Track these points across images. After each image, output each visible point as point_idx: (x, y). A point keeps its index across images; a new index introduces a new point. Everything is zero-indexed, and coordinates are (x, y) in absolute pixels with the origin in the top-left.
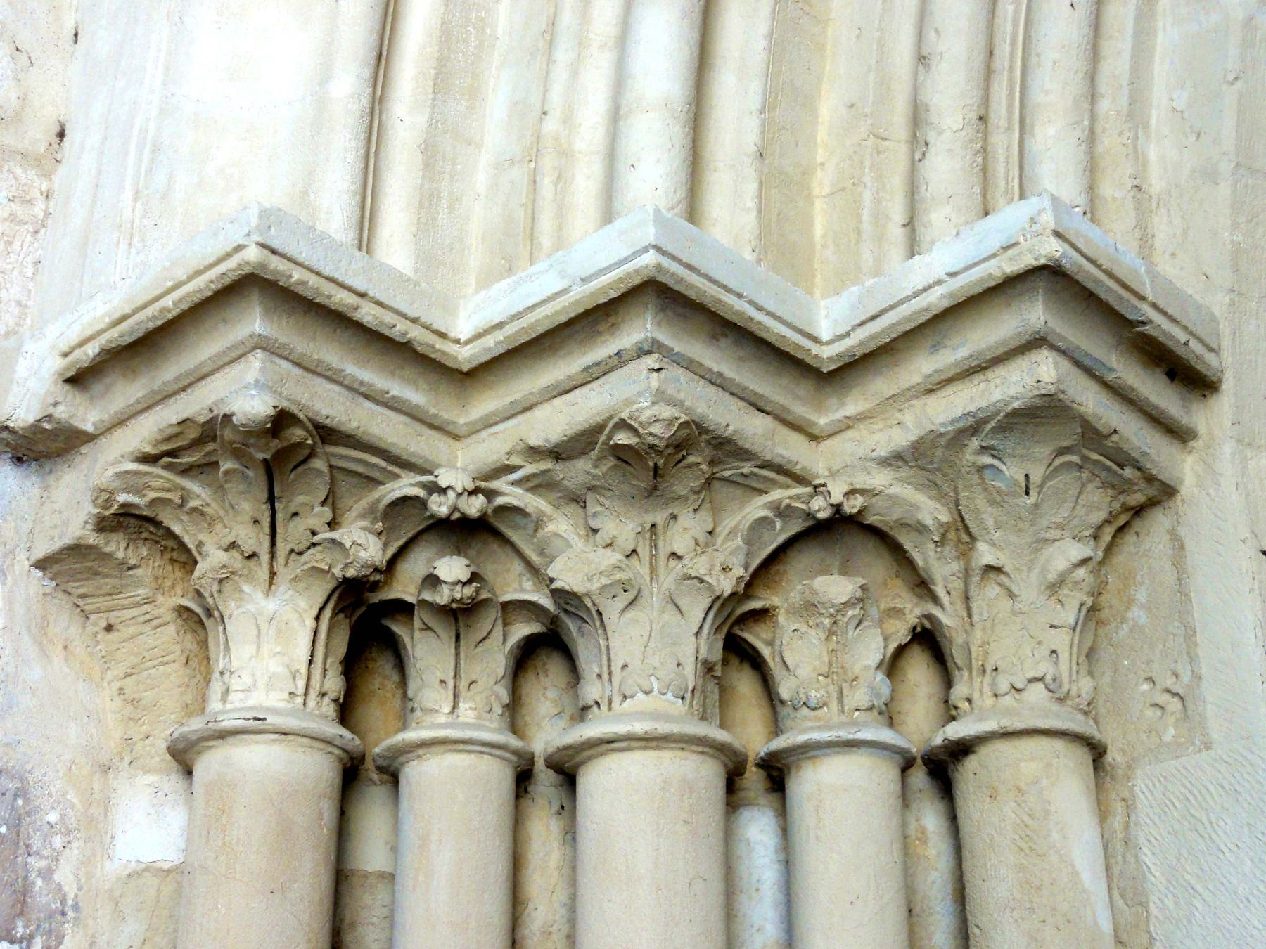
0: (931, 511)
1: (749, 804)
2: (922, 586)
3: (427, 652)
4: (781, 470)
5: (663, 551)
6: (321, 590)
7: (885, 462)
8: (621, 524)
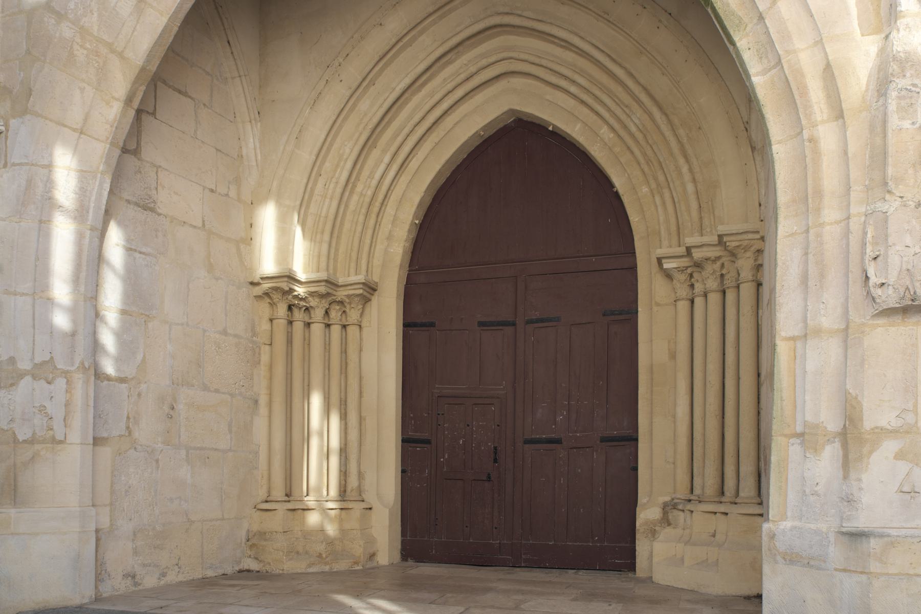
3: (296, 311)
8: (317, 300)
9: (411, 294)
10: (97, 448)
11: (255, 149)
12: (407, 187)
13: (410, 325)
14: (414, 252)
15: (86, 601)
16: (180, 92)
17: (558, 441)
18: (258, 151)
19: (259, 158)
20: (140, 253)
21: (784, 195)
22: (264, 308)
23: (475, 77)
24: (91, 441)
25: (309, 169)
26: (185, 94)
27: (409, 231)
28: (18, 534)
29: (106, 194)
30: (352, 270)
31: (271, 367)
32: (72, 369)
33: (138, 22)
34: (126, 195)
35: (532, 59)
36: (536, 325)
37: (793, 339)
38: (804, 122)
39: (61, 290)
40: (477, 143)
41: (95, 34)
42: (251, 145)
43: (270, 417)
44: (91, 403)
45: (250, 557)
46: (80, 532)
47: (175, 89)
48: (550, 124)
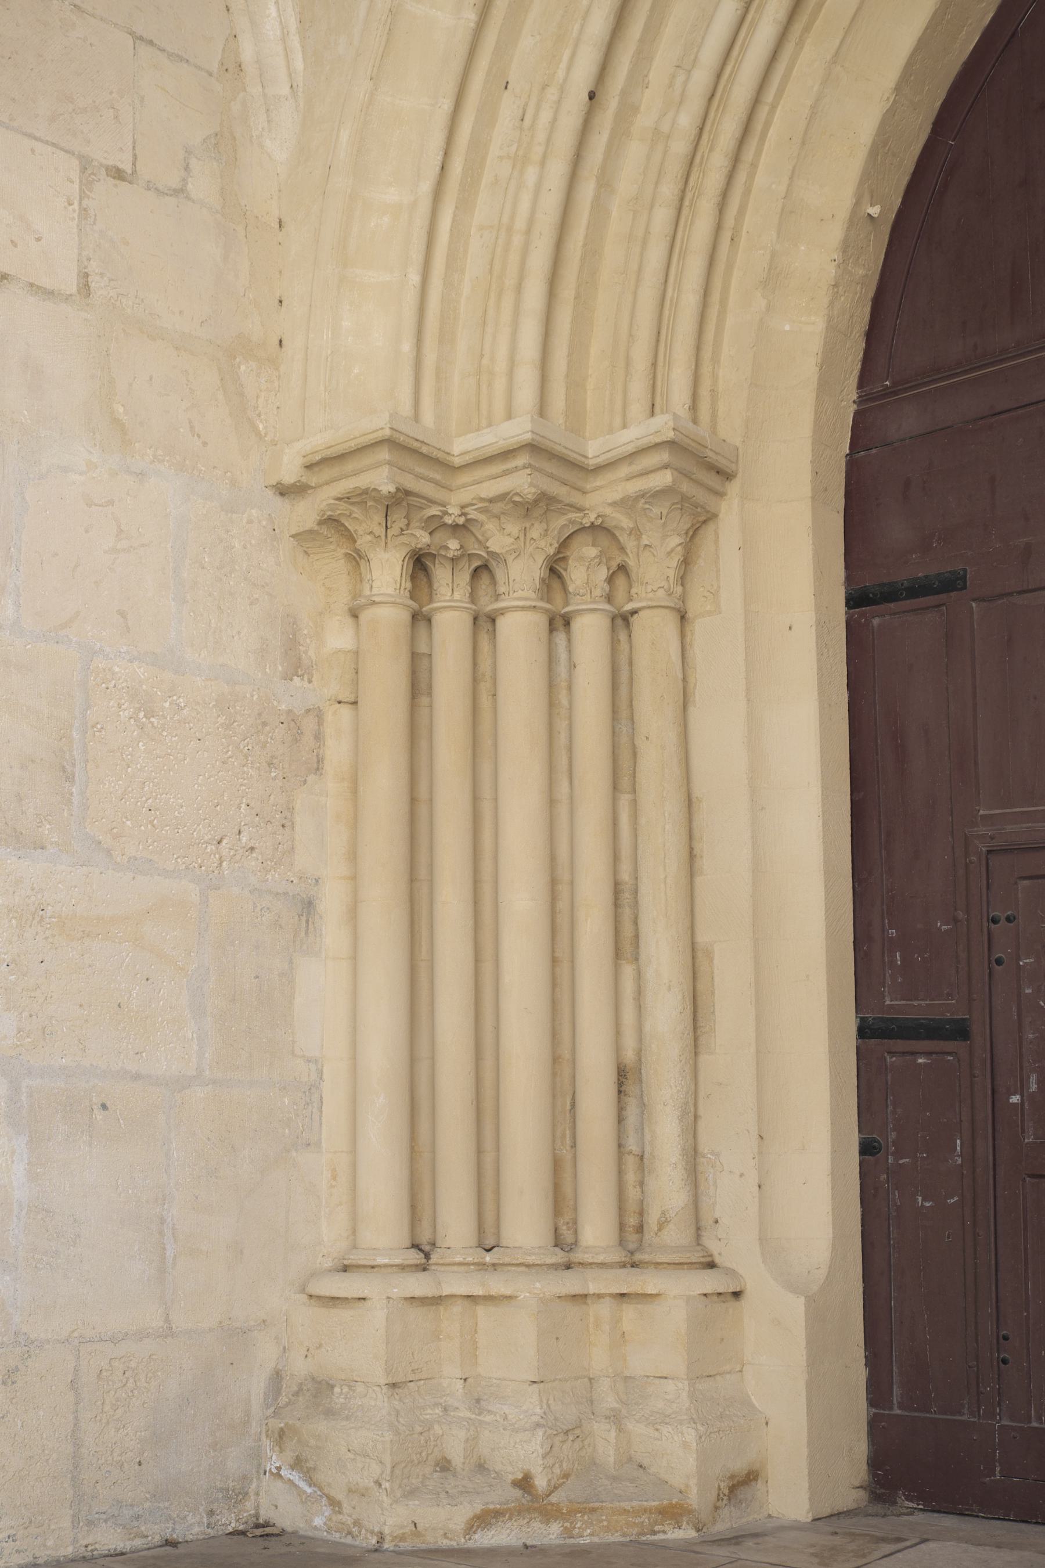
0: (626, 523)
1: (556, 630)
2: (622, 549)
3: (441, 574)
4: (571, 506)
5: (528, 537)
6: (404, 551)
7: (610, 504)
8: (513, 528)
13: (873, 596)
14: (872, 335)
18: (295, 42)
19: (299, 64)
25: (456, 66)
30: (637, 409)
42: (271, 28)
43: (354, 958)
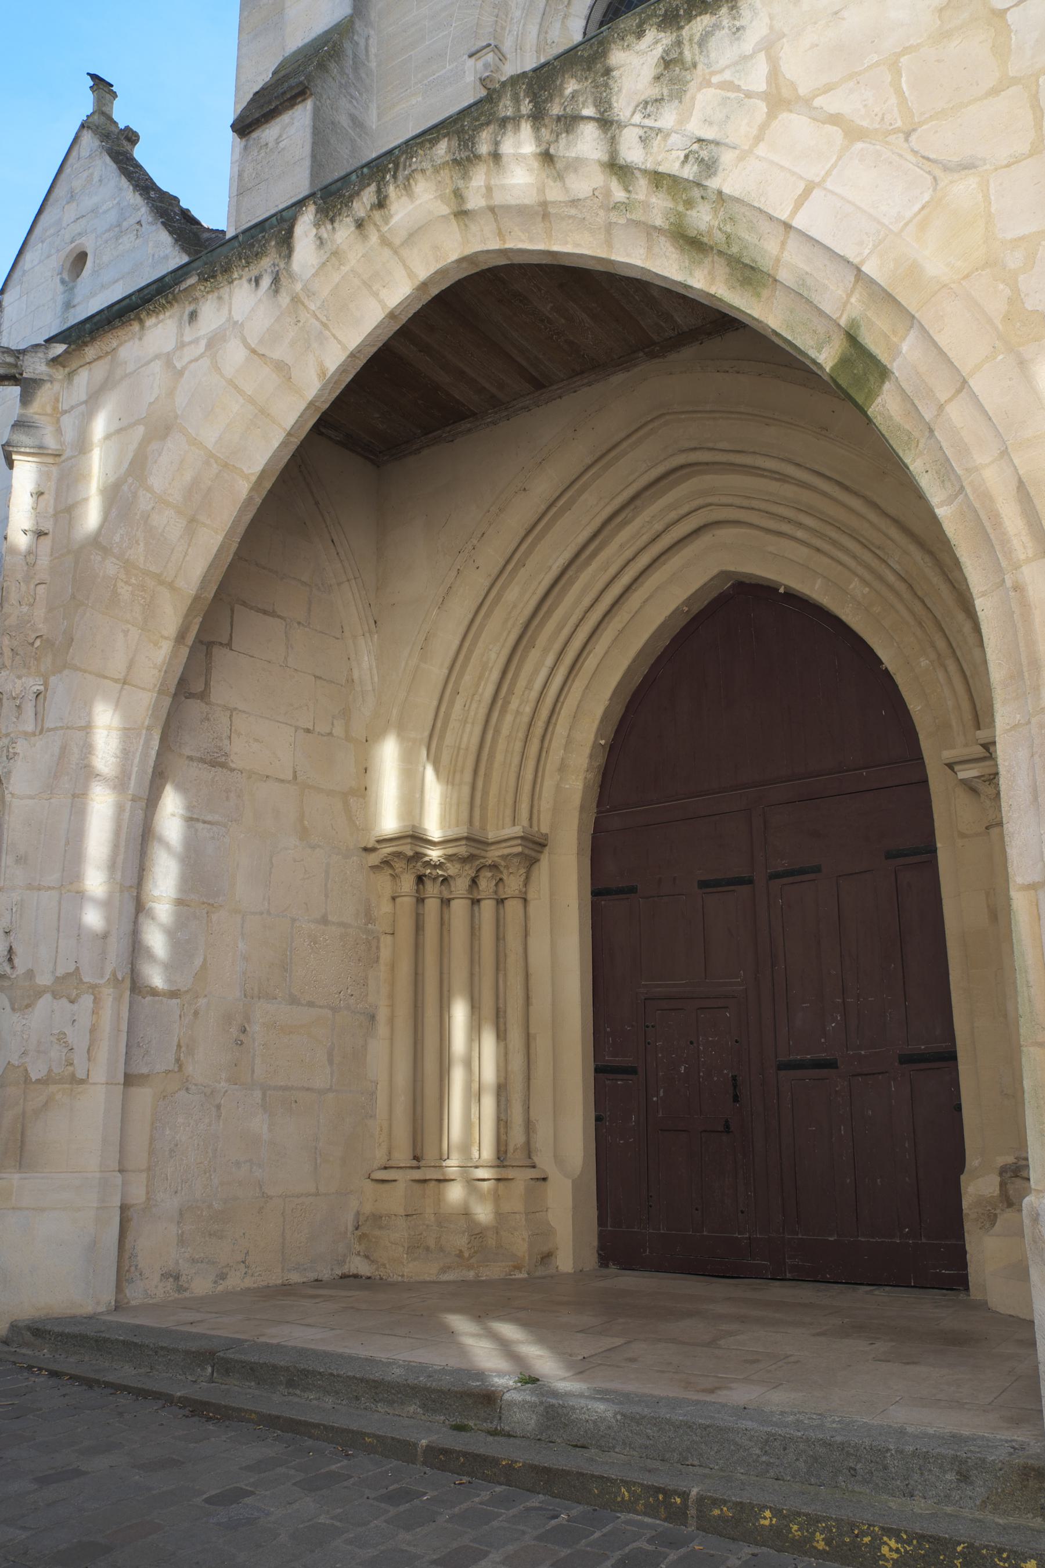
0: (503, 863)
3: (429, 884)
8: (458, 866)
9: (603, 845)
10: (133, 1090)
11: (371, 669)
12: (583, 696)
13: (605, 894)
15: (102, 1309)
16: (265, 612)
17: (831, 1064)
18: (375, 671)
19: (376, 679)
20: (204, 822)
21: (997, 673)
22: (383, 882)
23: (663, 536)
24: (121, 1079)
26: (273, 614)
27: (591, 756)
28: (20, 1209)
29: (153, 753)
30: (508, 820)
31: (393, 967)
32: (101, 982)
33: (189, 545)
34: (187, 751)
35: (738, 501)
36: (785, 880)
37: (1032, 887)
38: (1004, 564)
39: (95, 881)
40: (683, 623)
41: (142, 566)
42: (365, 665)
44: (124, 1027)
45: (358, 1254)
46: (98, 1208)
47: (259, 610)
48: (781, 585)
